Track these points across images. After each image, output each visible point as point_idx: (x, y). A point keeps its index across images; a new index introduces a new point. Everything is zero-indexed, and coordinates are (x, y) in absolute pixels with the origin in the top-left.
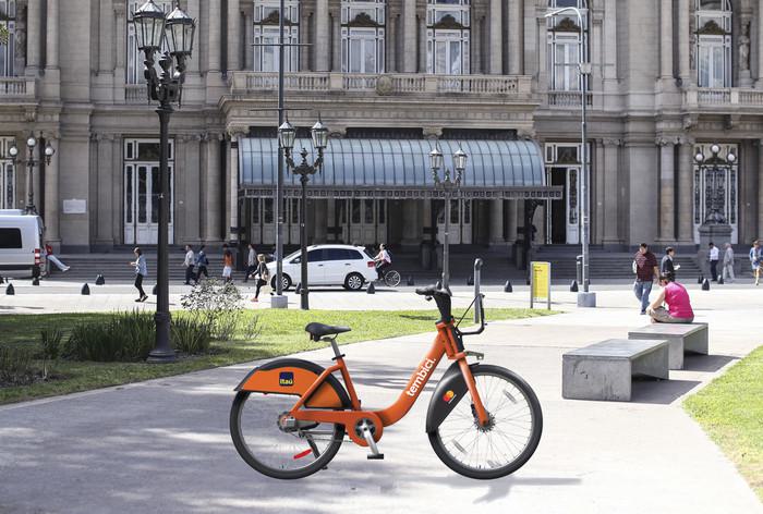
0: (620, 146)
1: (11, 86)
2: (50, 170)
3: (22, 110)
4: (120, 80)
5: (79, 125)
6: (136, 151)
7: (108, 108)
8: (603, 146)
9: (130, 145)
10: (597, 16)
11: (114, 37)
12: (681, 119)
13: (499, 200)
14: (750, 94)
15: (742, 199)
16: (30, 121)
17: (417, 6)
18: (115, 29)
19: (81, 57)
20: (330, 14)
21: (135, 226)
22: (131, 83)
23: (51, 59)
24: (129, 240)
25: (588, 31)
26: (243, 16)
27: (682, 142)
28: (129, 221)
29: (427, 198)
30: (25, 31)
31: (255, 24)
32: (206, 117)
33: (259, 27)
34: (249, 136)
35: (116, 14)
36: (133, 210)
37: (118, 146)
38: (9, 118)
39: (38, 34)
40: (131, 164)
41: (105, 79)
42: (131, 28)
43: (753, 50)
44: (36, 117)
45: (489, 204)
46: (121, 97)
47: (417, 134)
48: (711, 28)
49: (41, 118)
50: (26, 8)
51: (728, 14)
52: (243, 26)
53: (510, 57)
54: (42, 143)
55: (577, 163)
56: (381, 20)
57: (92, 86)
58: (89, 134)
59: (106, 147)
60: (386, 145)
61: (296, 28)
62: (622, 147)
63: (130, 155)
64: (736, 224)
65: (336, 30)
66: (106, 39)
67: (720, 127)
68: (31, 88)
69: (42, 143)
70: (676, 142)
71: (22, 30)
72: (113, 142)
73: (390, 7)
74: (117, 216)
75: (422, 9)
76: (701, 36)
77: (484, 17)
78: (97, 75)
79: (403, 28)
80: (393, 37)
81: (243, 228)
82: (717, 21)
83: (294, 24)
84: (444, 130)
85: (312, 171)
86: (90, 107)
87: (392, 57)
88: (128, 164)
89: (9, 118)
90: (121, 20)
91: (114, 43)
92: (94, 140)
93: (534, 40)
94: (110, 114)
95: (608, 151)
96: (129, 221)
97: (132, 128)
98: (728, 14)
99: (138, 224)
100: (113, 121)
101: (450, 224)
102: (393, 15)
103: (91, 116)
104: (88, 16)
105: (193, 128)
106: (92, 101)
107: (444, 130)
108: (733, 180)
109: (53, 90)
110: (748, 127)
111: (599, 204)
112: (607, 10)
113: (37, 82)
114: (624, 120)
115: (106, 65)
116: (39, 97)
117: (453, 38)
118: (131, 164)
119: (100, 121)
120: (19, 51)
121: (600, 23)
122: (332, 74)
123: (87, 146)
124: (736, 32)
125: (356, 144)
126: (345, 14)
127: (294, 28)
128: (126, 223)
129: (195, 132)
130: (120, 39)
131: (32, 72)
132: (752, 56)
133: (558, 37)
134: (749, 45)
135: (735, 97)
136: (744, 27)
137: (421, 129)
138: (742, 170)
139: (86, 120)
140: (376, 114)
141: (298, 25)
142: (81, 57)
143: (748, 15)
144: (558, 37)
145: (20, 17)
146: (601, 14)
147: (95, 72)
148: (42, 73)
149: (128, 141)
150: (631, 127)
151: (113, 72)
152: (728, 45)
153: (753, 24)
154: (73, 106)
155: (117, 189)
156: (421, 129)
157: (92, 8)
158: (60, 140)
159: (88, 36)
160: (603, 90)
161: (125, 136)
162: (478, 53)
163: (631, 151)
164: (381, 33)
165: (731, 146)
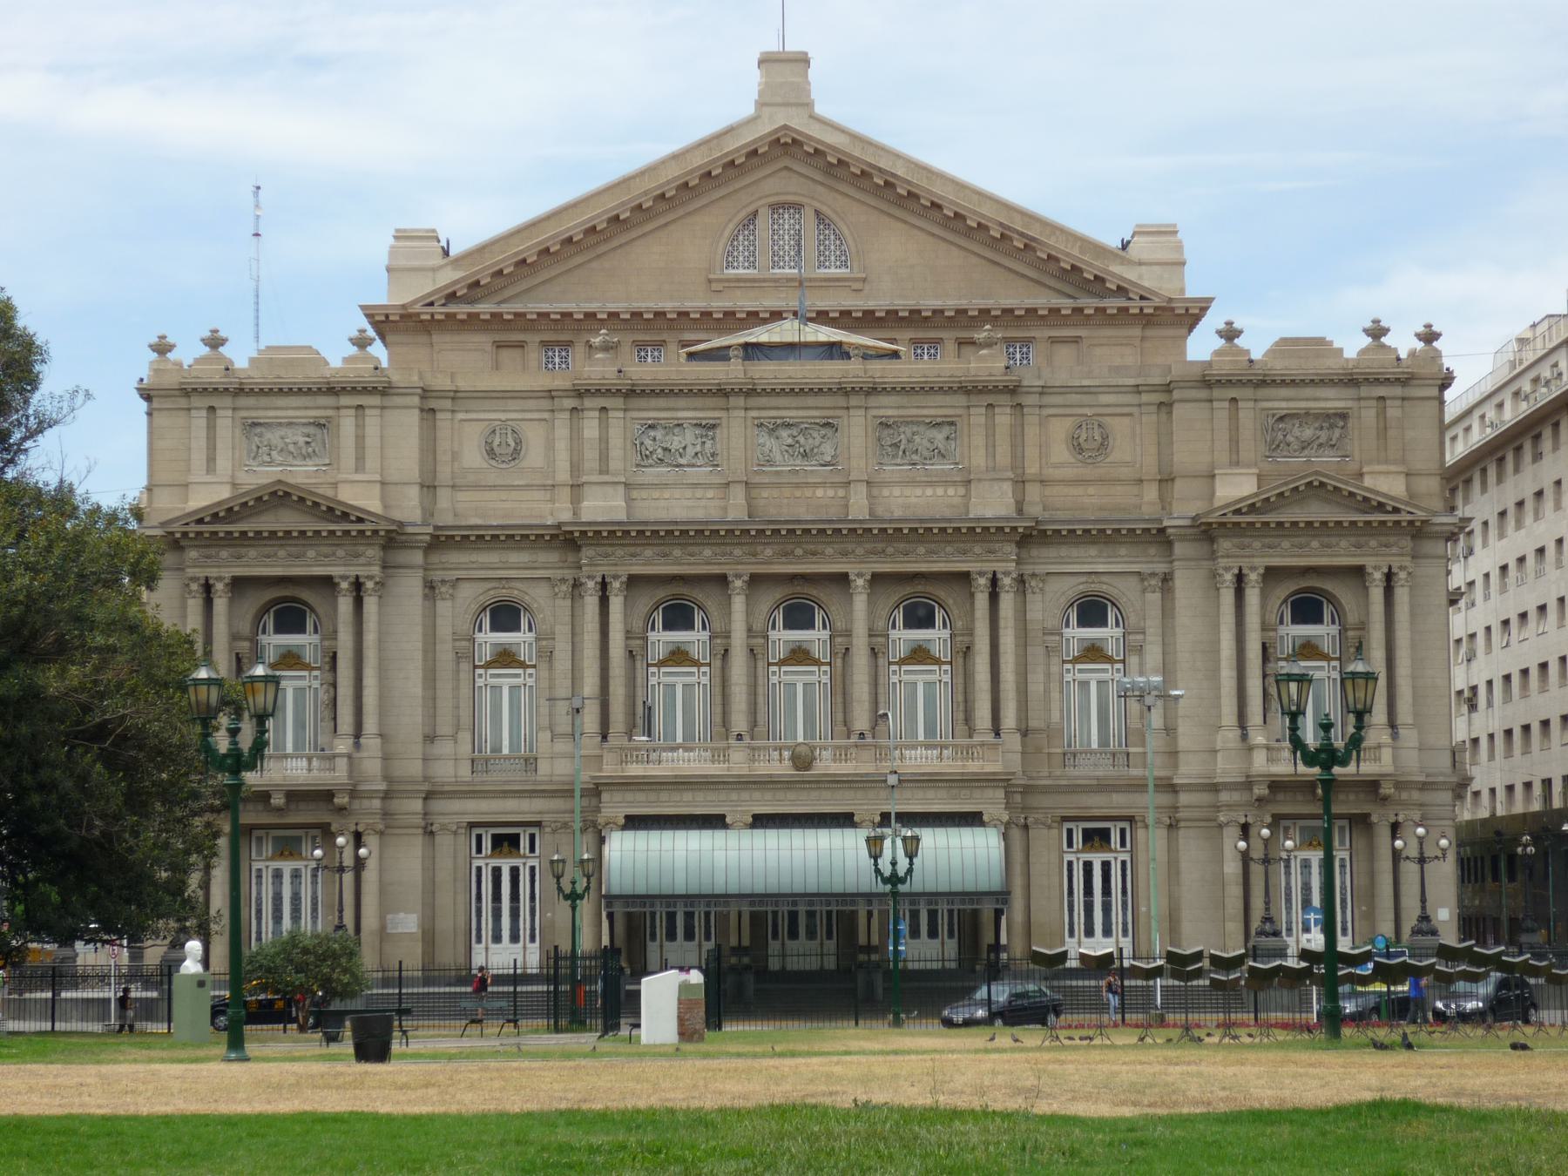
0: (1170, 826)
1: (315, 763)
2: (370, 875)
4: (465, 748)
7: (447, 788)
12: (1248, 784)
13: (802, 909)
14: (969, 747)
18: (456, 679)
20: (1264, 644)
24: (774, 964)
25: (1123, 661)
27: (1250, 820)
29: (785, 909)
30: (334, 685)
35: (458, 657)
39: (1234, 674)
40: (481, 863)
41: (444, 748)
45: (975, 914)
47: (714, 822)
49: (356, 805)
50: (335, 654)
54: (358, 840)
60: (667, 835)
61: (706, 669)
62: (1172, 827)
64: (1130, 938)
65: (881, 671)
69: (358, 840)
70: (1242, 820)
72: (455, 833)
74: (461, 939)
75: (1271, 634)
80: (839, 679)
81: (746, 948)
84: (627, 817)
86: (426, 787)
87: (840, 707)
91: (456, 697)
94: (1046, 790)
96: (479, 940)
98: (1334, 630)
100: (456, 805)
103: (425, 799)
104: (419, 664)
106: (426, 779)
107: (627, 817)
109: (372, 766)
111: (1143, 909)
112: (1150, 631)
114: (1214, 788)
115: (444, 728)
117: (688, 680)
118: (481, 863)
119: (438, 805)
120: (326, 713)
121: (1140, 650)
125: (641, 835)
127: (824, 668)
128: (474, 945)
130: (465, 691)
133: (1080, 671)
135: (609, 758)
137: (852, 815)
142: (410, 721)
143: (1357, 633)
144: (1080, 671)
146: (1140, 637)
147: (430, 738)
150: (1184, 798)
151: (454, 738)
155: (461, 898)
163: (1181, 832)
164: (1334, 668)
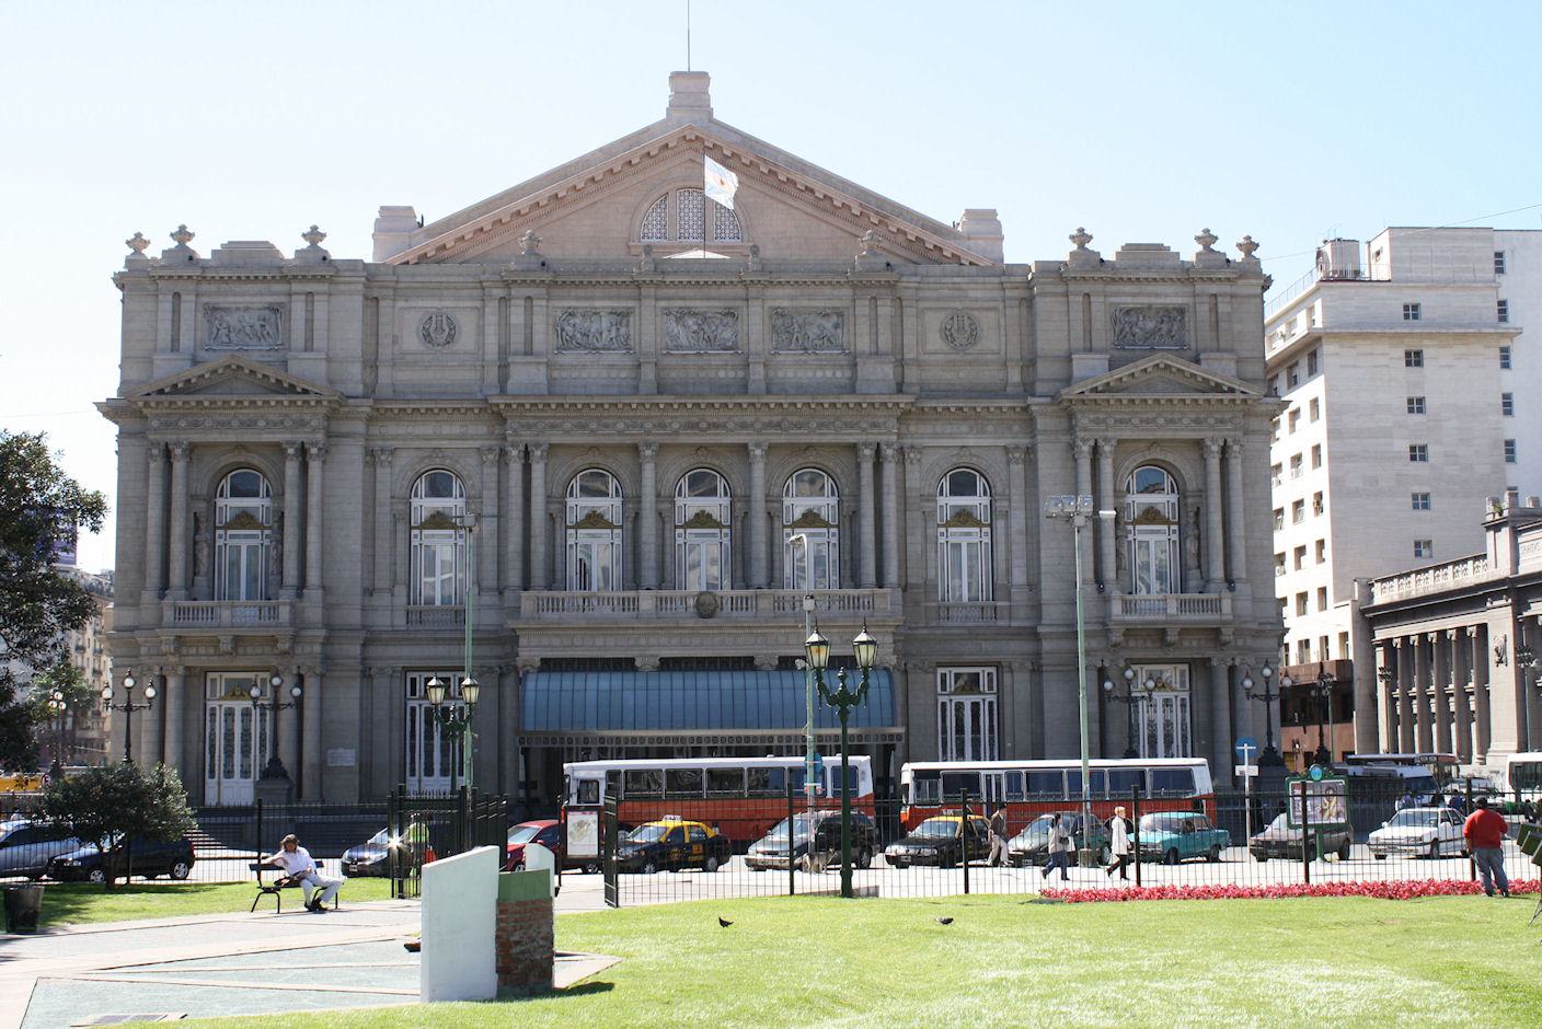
3: (273, 641)
4: (401, 600)
5: (348, 657)
6: (951, 684)
8: (1012, 672)
9: (944, 676)
10: (1001, 505)
11: (394, 546)
15: (1195, 735)
16: (284, 653)
17: (767, 501)
19: (350, 574)
21: (420, 781)
22: (415, 603)
23: (313, 577)
25: (991, 526)
26: (551, 518)
28: (212, 776)
31: (939, 526)
32: (504, 644)
33: (682, 531)
34: (541, 670)
36: (217, 762)
37: (397, 683)
38: (259, 651)
41: (382, 600)
42: (416, 536)
43: (1203, 543)
44: (292, 648)
46: (400, 621)
48: (1151, 516)
51: (1173, 498)
52: (771, 530)
53: (886, 564)
55: (980, 693)
56: (726, 520)
57: (364, 609)
58: (360, 668)
59: (381, 684)
61: (620, 531)
63: (944, 688)
66: (383, 545)
67: (1158, 645)
68: (284, 613)
70: (1100, 665)
71: (277, 541)
73: (1185, 497)
76: (1138, 527)
77: (637, 514)
78: (371, 595)
79: (1233, 523)
82: (1160, 508)
83: (616, 527)
85: (855, 700)
88: (411, 704)
89: (259, 651)
90: (401, 527)
92: (366, 674)
93: (919, 539)
95: (1017, 676)
96: (212, 776)
97: (416, 659)
98: (1173, 498)
99: (223, 780)
100: (392, 651)
101: (223, 780)
102: (739, 513)
105: (491, 658)
106: (364, 627)
108: (1183, 711)
109: (314, 613)
110: (1195, 643)
113: (292, 605)
115: (383, 581)
116: (298, 625)
117: (253, 542)
119: (375, 651)
122: (281, 592)
123: (357, 684)
124: (1183, 522)
126: (788, 513)
128: (208, 780)
129: (494, 663)
130: (401, 548)
131: (286, 596)
132: (1203, 551)
134: (1199, 538)
136: (1192, 514)
138: (1194, 699)
139: (356, 650)
140: (696, 641)
141: (622, 527)
142: (350, 574)
143: (1196, 500)
145: (276, 526)
147: (369, 592)
148: (300, 595)
149: (410, 675)
152: (1175, 537)
153: (1202, 511)
154: (309, 633)
156: (632, 660)
157: (365, 514)
158: (322, 676)
159: (358, 548)
160: (1010, 600)
161: (406, 670)
162: (847, 557)
165: (1180, 667)
